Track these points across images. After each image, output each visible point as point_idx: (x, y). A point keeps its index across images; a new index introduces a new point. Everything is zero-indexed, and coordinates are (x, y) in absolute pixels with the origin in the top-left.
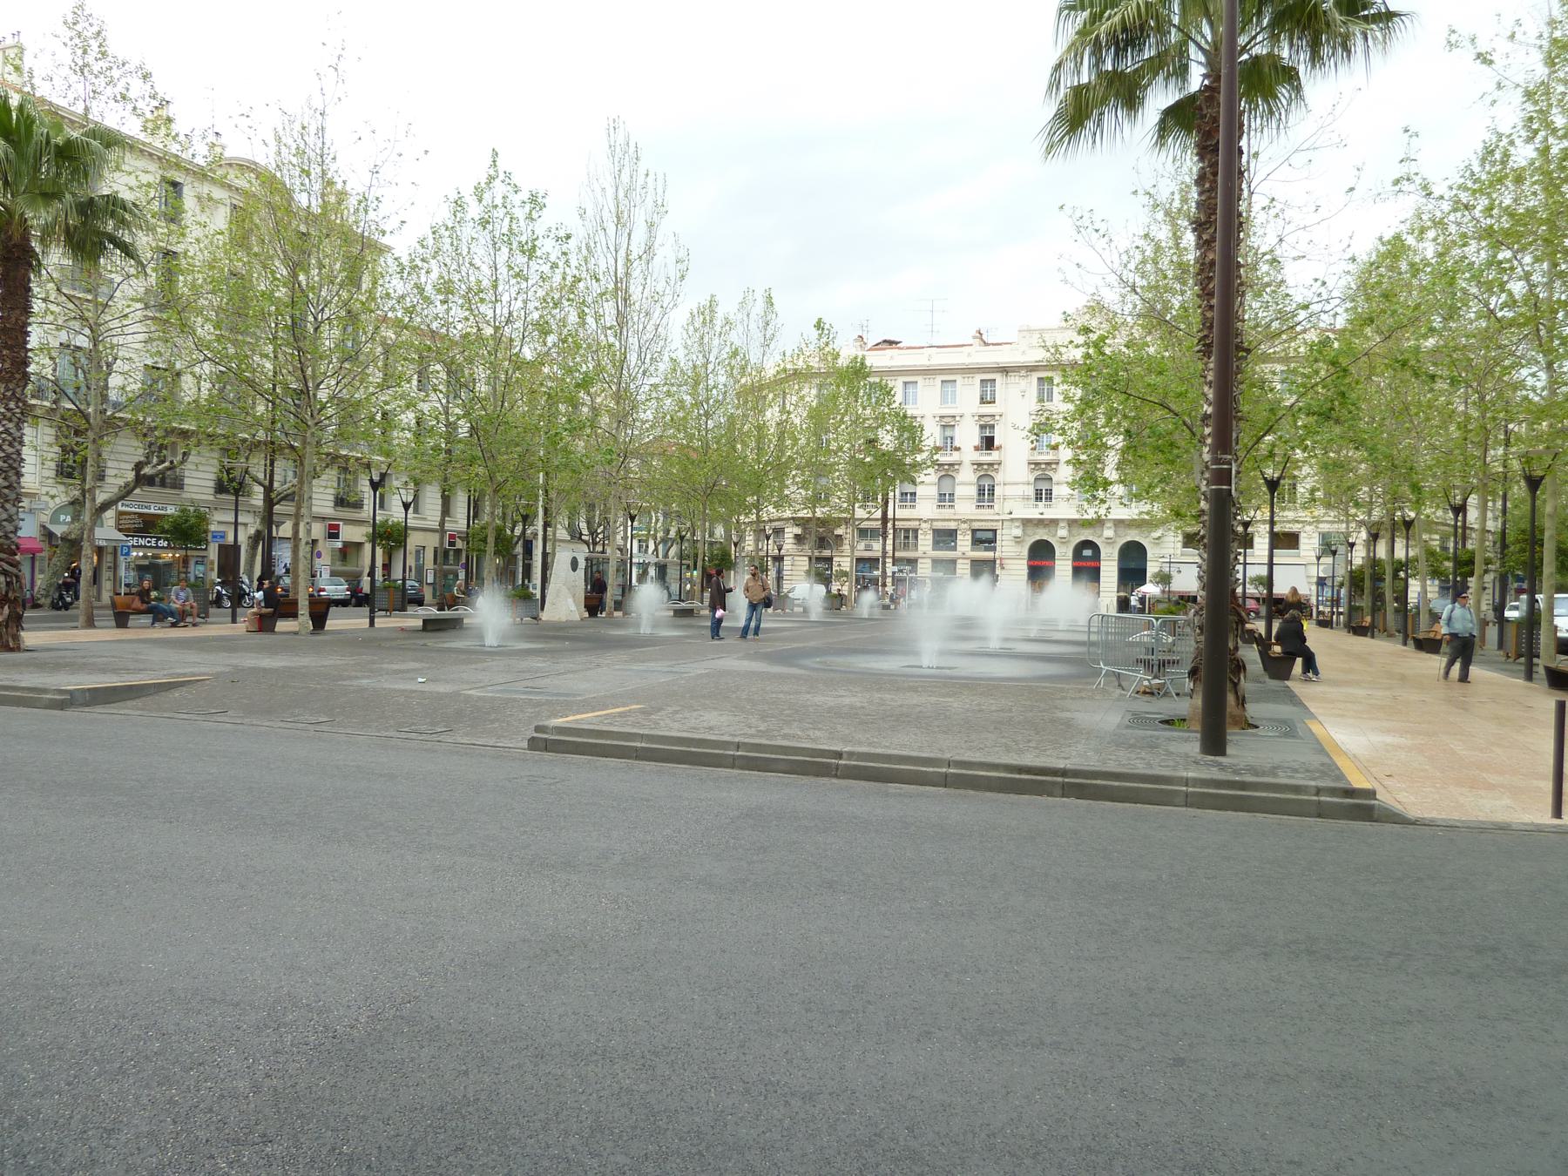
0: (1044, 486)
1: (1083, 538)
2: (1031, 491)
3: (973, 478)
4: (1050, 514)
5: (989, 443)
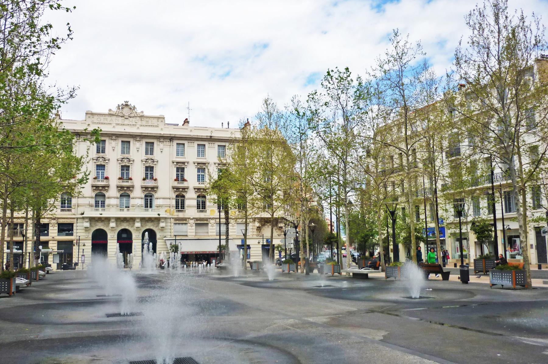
1: (123, 228)
2: (93, 202)
3: (195, 196)
4: (105, 214)
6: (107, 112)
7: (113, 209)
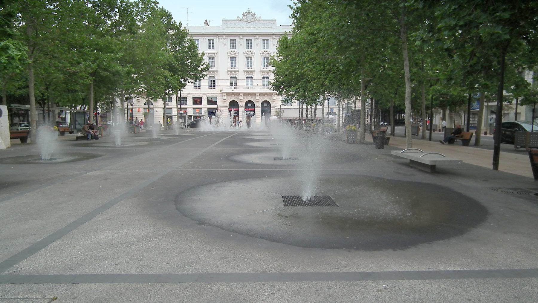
0: (234, 80)
4: (236, 91)
5: (233, 58)
6: (236, 19)
7: (241, 89)
